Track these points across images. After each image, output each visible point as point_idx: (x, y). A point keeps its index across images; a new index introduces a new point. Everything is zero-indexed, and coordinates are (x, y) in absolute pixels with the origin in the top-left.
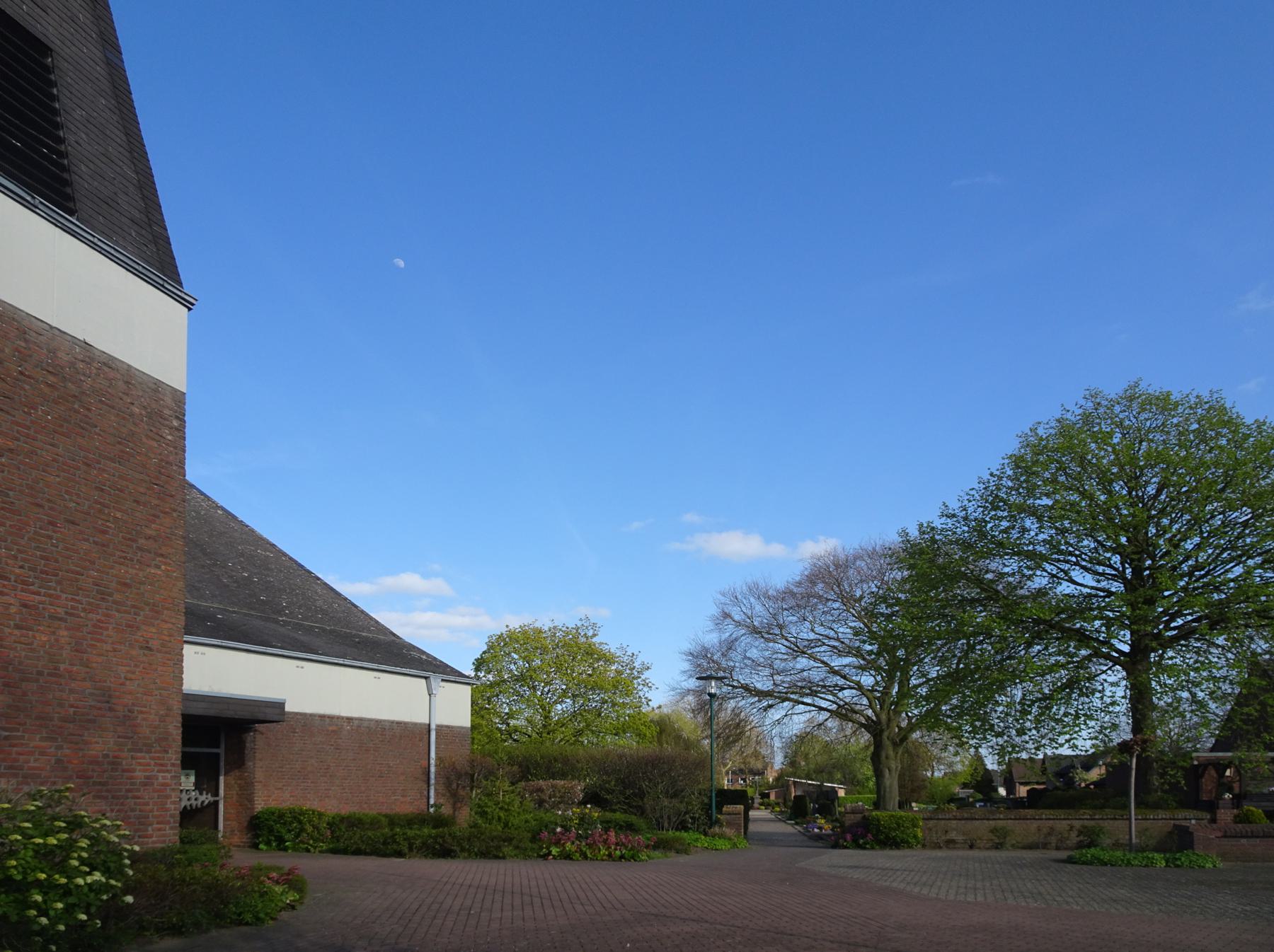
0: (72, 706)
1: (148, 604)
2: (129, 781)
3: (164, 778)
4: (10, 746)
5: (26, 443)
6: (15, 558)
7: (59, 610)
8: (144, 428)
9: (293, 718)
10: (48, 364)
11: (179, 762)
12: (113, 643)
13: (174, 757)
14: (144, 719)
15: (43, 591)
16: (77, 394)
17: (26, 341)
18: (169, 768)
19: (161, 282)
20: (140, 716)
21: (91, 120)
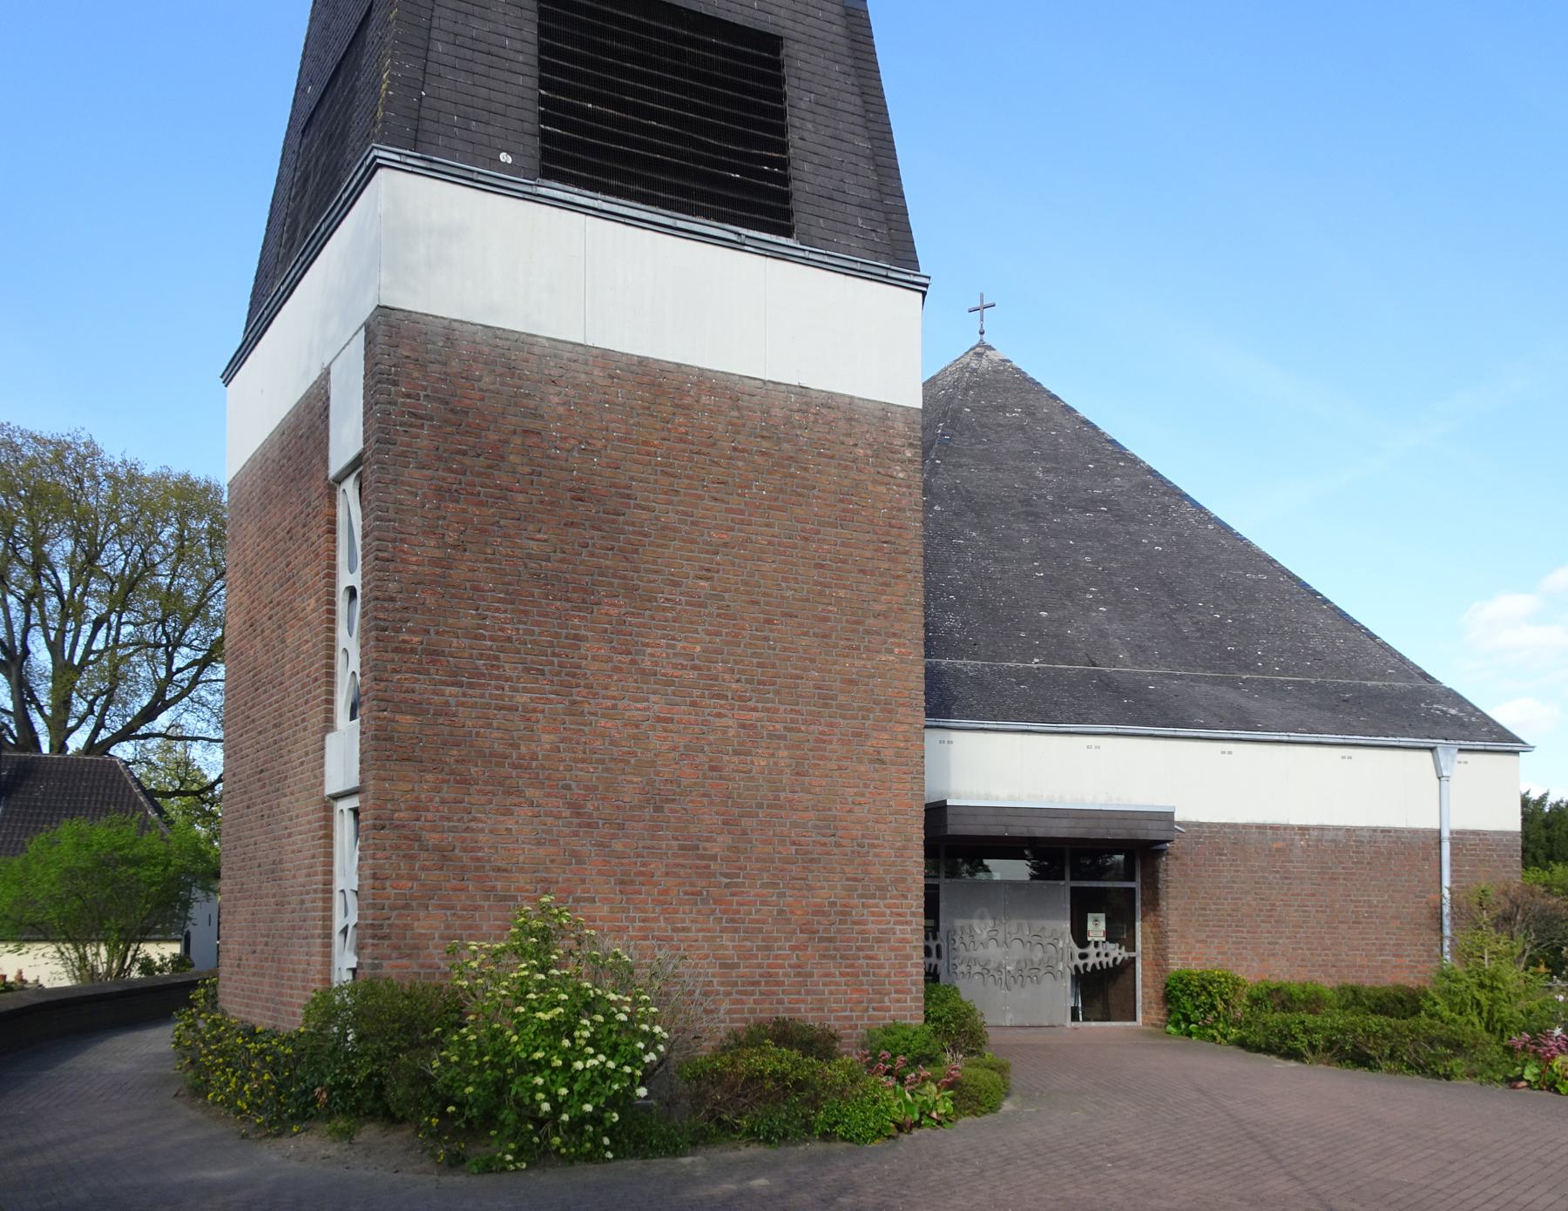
0: (794, 843)
1: (876, 703)
2: (860, 936)
3: (902, 932)
4: (731, 895)
5: (741, 531)
6: (732, 671)
7: (778, 726)
8: (870, 472)
9: (1219, 832)
10: (762, 428)
11: (922, 910)
12: (839, 759)
13: (915, 903)
14: (876, 855)
15: (760, 705)
16: (793, 455)
17: (739, 409)
18: (909, 918)
19: (884, 272)
20: (873, 851)
21: (822, 100)
